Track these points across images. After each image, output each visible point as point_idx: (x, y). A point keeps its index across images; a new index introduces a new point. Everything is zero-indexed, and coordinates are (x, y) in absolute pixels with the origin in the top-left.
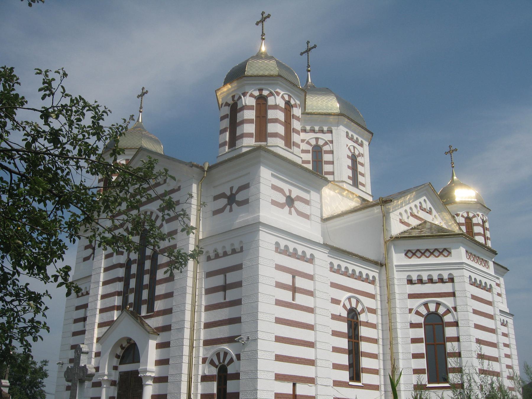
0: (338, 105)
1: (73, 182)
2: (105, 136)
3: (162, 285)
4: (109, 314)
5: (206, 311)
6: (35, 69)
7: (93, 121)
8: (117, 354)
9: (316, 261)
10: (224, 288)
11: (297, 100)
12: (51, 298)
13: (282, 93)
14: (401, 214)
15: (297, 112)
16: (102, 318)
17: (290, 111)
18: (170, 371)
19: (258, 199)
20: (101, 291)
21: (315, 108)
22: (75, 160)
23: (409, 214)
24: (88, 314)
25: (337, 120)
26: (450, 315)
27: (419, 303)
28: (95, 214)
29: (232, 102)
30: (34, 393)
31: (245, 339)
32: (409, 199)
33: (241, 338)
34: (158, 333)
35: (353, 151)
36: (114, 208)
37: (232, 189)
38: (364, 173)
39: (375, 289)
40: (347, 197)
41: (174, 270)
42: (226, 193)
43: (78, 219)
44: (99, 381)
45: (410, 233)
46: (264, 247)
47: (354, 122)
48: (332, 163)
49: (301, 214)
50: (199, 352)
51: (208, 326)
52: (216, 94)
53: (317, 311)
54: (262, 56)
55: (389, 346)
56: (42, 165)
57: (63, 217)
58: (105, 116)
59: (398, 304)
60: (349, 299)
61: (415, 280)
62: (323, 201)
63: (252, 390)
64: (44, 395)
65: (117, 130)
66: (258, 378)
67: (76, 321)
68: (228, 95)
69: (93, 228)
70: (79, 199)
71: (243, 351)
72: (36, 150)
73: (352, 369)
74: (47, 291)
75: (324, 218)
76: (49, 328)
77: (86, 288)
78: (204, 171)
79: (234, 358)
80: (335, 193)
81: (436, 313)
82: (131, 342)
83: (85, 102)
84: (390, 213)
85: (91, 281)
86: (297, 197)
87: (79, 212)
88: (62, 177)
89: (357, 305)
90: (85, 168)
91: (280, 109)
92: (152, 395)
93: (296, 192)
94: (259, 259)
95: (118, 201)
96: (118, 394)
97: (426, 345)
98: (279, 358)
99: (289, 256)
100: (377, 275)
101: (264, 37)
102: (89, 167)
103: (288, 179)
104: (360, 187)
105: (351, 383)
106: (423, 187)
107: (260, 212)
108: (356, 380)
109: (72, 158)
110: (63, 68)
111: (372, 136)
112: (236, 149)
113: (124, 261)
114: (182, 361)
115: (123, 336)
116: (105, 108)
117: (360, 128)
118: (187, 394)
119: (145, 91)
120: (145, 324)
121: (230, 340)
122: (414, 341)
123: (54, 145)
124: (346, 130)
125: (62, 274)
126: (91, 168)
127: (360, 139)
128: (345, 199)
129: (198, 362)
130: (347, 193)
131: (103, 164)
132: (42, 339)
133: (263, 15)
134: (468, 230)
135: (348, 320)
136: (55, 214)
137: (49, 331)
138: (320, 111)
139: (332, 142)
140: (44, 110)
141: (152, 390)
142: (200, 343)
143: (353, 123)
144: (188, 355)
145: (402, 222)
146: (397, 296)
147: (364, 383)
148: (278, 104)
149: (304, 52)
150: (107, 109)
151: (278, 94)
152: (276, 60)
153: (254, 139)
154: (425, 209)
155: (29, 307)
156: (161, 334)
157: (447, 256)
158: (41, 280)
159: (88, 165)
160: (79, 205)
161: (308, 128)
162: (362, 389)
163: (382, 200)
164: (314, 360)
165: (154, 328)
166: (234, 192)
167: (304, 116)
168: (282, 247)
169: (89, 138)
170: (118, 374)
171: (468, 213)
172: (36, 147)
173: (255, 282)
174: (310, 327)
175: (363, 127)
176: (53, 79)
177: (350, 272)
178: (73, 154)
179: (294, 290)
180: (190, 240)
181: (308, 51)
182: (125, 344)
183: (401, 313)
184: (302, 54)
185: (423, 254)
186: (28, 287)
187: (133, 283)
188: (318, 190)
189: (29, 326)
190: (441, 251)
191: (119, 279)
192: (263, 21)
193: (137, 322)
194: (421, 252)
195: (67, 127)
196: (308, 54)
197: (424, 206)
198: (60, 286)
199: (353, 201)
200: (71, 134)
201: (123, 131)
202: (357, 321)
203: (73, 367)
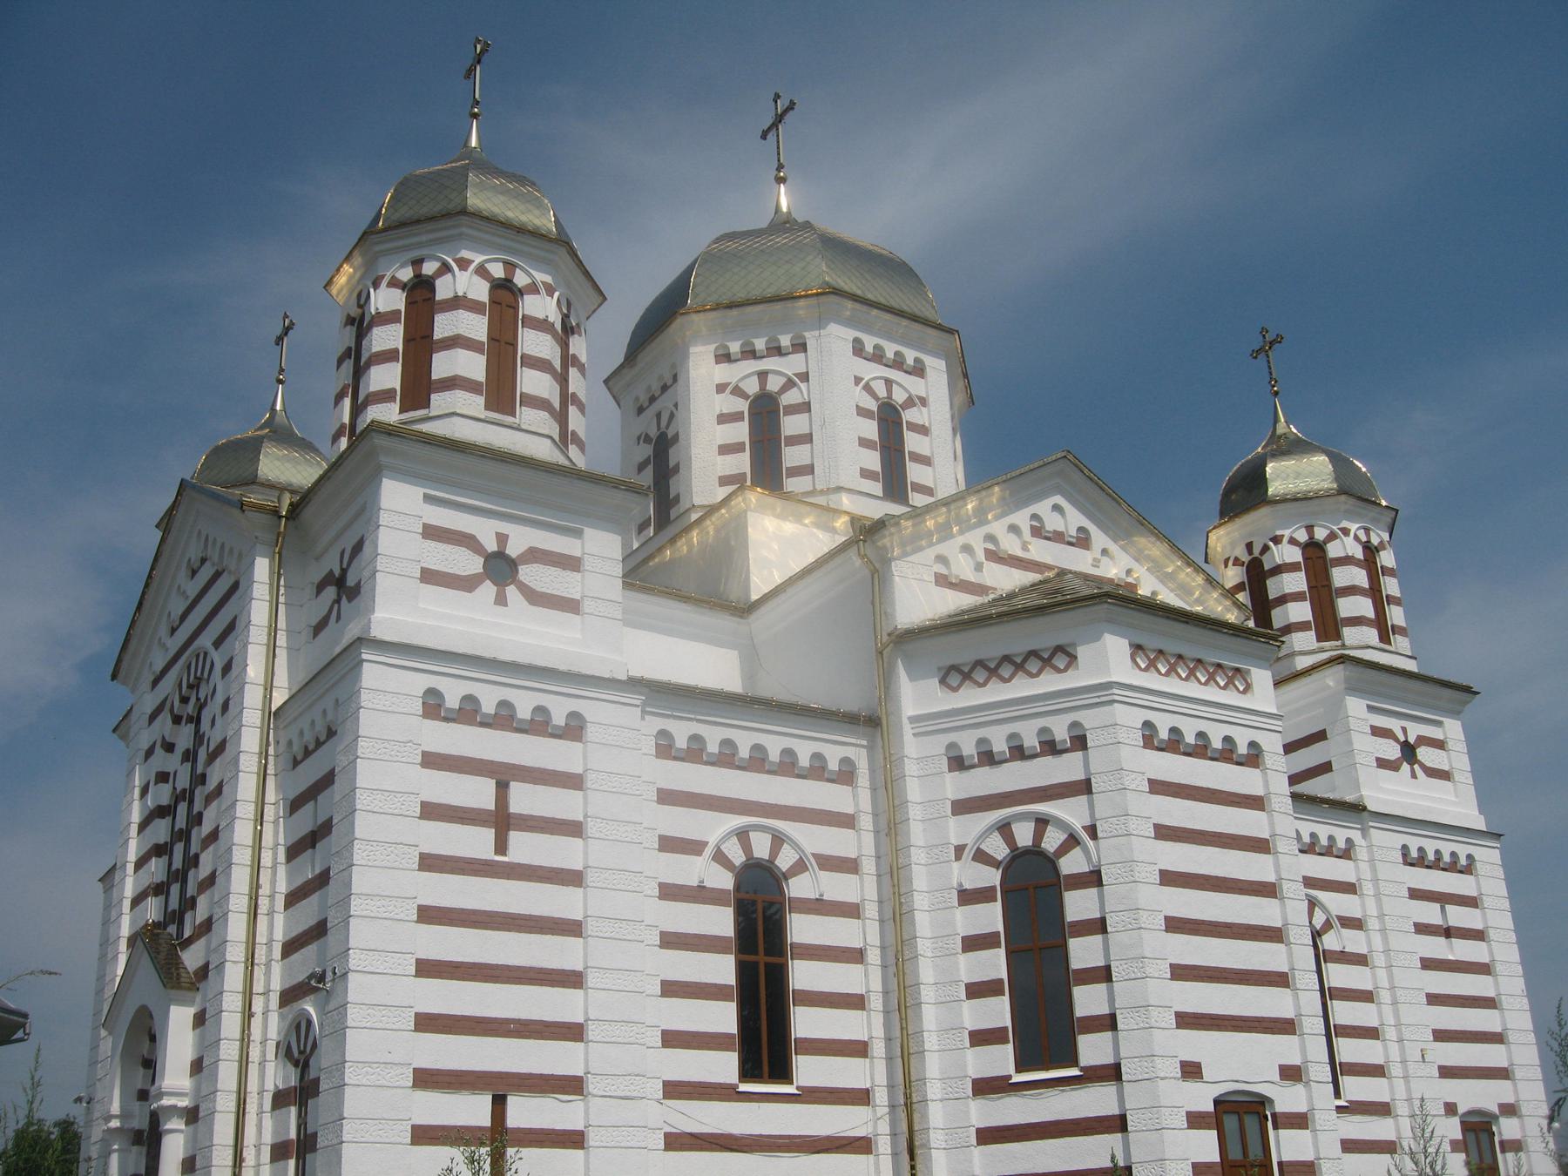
9: (591, 732)
11: (533, 269)
17: (514, 308)
23: (981, 556)
26: (1076, 852)
27: (983, 825)
39: (855, 796)
49: (535, 598)
60: (743, 835)
78: (280, 517)
80: (800, 527)
81: (1035, 851)
91: (475, 307)
97: (1009, 954)
105: (744, 1087)
117: (905, 322)
124: (851, 334)
127: (910, 356)
134: (1314, 584)
139: (805, 377)
145: (942, 581)
147: (801, 1084)
148: (460, 294)
149: (770, 129)
153: (396, 407)
157: (1065, 670)
161: (735, 347)
171: (1310, 529)
190: (966, 670)
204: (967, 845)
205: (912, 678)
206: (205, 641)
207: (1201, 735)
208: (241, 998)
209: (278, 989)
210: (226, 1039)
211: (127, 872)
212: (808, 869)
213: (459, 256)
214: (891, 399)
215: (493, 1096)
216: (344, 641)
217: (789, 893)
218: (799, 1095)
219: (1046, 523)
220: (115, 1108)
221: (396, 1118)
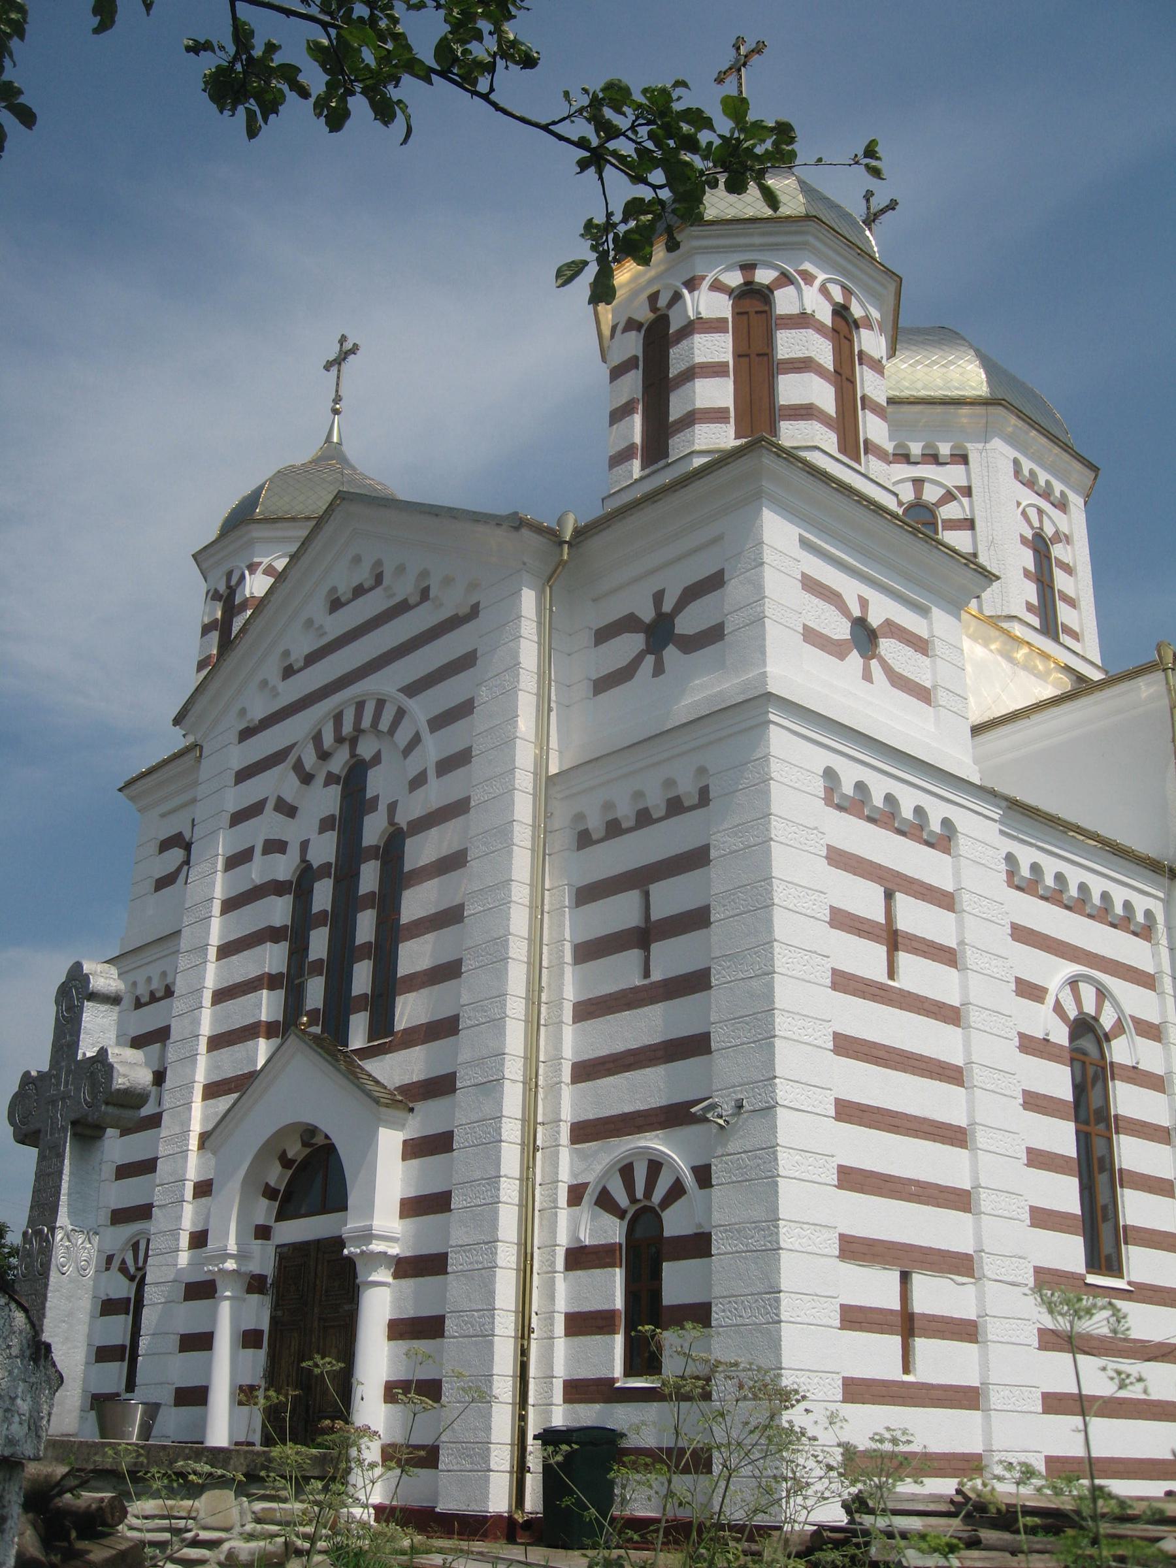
4: (238, 1050)
5: (579, 1021)
9: (963, 844)
13: (821, 277)
16: (218, 1067)
17: (849, 340)
19: (759, 620)
20: (212, 976)
21: (907, 384)
25: (985, 421)
29: (651, 316)
31: (727, 1108)
33: (713, 1107)
34: (411, 1105)
35: (1036, 524)
37: (658, 597)
38: (1074, 596)
39: (1155, 955)
40: (1027, 668)
42: (637, 613)
44: (209, 1277)
50: (555, 1165)
51: (586, 1071)
60: (1073, 983)
63: (759, 1293)
66: (780, 1248)
71: (719, 1152)
77: (164, 974)
79: (689, 1179)
82: (314, 1141)
89: (1099, 1007)
92: (390, 1320)
93: (881, 610)
94: (769, 823)
96: (274, 1320)
103: (855, 560)
105: (1092, 1279)
107: (769, 661)
112: (669, 465)
117: (1057, 450)
119: (350, 346)
127: (1058, 487)
128: (1022, 673)
129: (555, 1201)
130: (1026, 655)
139: (968, 491)
141: (392, 1302)
142: (558, 1133)
143: (1034, 433)
144: (518, 1176)
148: (809, 311)
151: (809, 278)
153: (730, 429)
156: (419, 1106)
162: (1130, 1300)
165: (396, 1089)
166: (667, 607)
168: (848, 789)
173: (762, 907)
177: (1073, 891)
182: (295, 1150)
187: (319, 944)
191: (272, 934)
199: (1045, 681)
206: (386, 682)
209: (569, 1119)
210: (505, 1176)
213: (801, 268)
214: (1042, 530)
215: (902, 1272)
216: (687, 701)
218: (1131, 1291)
220: (232, 1248)
221: (826, 1294)
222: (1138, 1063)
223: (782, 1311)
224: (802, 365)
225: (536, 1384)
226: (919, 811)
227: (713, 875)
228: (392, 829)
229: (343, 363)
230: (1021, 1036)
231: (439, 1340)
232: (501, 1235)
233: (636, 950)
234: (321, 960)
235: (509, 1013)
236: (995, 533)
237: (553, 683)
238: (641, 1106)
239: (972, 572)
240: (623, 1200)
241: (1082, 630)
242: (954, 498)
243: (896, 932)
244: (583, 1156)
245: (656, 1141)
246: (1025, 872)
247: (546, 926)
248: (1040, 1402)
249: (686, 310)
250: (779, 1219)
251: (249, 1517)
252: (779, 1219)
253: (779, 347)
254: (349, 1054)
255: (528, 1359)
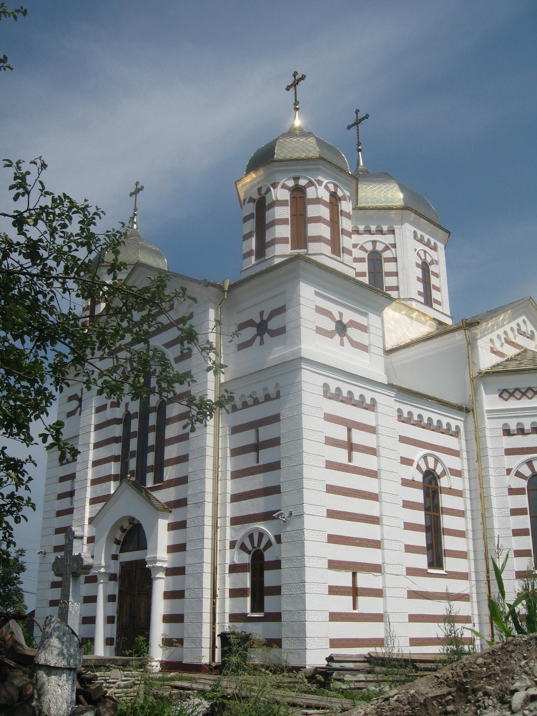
0: (401, 196)
1: (59, 310)
2: (100, 247)
3: (173, 446)
4: (103, 486)
6: (4, 160)
7: (81, 227)
8: (116, 539)
9: (379, 408)
10: (257, 447)
12: (36, 465)
14: (492, 341)
15: (346, 206)
17: (337, 206)
18: (188, 559)
19: (298, 327)
22: (60, 280)
23: (503, 341)
24: (76, 487)
25: (401, 216)
28: (88, 351)
30: (9, 592)
31: (286, 515)
32: (503, 320)
33: (281, 514)
34: (170, 510)
35: (423, 258)
36: (111, 344)
37: (262, 313)
39: (460, 443)
40: (417, 320)
41: (195, 423)
43: (65, 360)
44: (94, 574)
45: (505, 366)
46: (308, 390)
47: (423, 218)
48: (396, 274)
49: (355, 344)
50: (225, 533)
51: (236, 498)
52: (236, 186)
53: (383, 474)
54: (296, 133)
55: (480, 520)
56: (16, 289)
57: (46, 358)
58: (97, 220)
59: (491, 463)
60: (425, 457)
61: (514, 430)
62: (385, 327)
64: (22, 594)
65: (113, 237)
66: (305, 567)
67: (61, 496)
68: (252, 187)
69: (86, 371)
70: (68, 334)
71: (284, 531)
72: (8, 269)
73: (430, 551)
74: (30, 457)
75: (387, 349)
76: (35, 505)
79: (273, 540)
80: (400, 315)
83: (71, 202)
84: (477, 339)
85: (78, 443)
86: (351, 321)
87: (66, 350)
88: (44, 303)
90: (74, 291)
91: (324, 203)
92: (164, 592)
93: (348, 316)
95: (120, 333)
96: (120, 591)
98: (333, 539)
99: (342, 401)
100: (461, 425)
101: (297, 106)
102: (80, 289)
104: (435, 306)
105: (430, 571)
106: (521, 303)
108: (437, 567)
109: (56, 278)
110: (41, 157)
111: (449, 236)
113: (122, 415)
114: (203, 546)
115: (120, 517)
116: (97, 209)
117: (432, 226)
118: (211, 589)
119: (140, 187)
120: (152, 498)
121: (267, 516)
122: (515, 512)
123: (32, 261)
124: (413, 229)
125: (53, 432)
126: (83, 290)
127: (433, 241)
128: (416, 322)
129: (225, 547)
131: (98, 284)
132: (27, 520)
133: (295, 77)
135: (424, 487)
136: (36, 354)
137: (34, 509)
138: (377, 204)
139: (394, 246)
140: (18, 215)
142: (226, 521)
143: (422, 220)
145: (494, 351)
146: (490, 453)
148: (320, 197)
149: (353, 125)
150: (100, 210)
151: (320, 183)
152: (315, 137)
153: (289, 246)
154: (524, 332)
155: (8, 479)
156: (173, 510)
158: (22, 442)
159: (79, 286)
160: (68, 340)
161: (362, 228)
163: (466, 322)
164: (380, 541)
165: (165, 503)
167: (355, 211)
168: (333, 390)
169: (76, 250)
170: (118, 565)
172: (8, 265)
173: (298, 439)
174: (373, 497)
175: (436, 225)
176: (28, 173)
178: (58, 273)
179: (350, 447)
180: (208, 384)
181: (357, 123)
182: (126, 526)
183: (496, 475)
184: (349, 127)
185: (524, 394)
186: (5, 451)
187: (134, 444)
188: (379, 311)
189: (8, 504)
190: (511, 391)
191: (115, 440)
192: (295, 84)
193: (141, 495)
194: (509, 393)
195: (48, 236)
196: (358, 127)
197: (523, 329)
198: (51, 448)
199: (425, 325)
200: (54, 245)
201: (122, 238)
202: (436, 487)
203: (64, 556)
204: (512, 469)
205: (486, 394)
207: (350, 393)
208: (211, 519)
210: (206, 538)
211: (90, 448)
212: (446, 475)
215: (353, 573)
217: (440, 484)
219: (521, 327)
220: (103, 564)
222: (451, 486)
223: (306, 589)
224: (317, 220)
225: (219, 615)
226: (362, 396)
227: (281, 426)
228: (161, 400)
229: (137, 194)
230: (402, 479)
231: (183, 599)
232: (205, 560)
233: (254, 453)
234: (135, 451)
235: (206, 476)
236: (405, 263)
237: (222, 346)
238: (256, 512)
239: (385, 298)
240: (250, 547)
241: (442, 301)
242: (389, 249)
243: (352, 444)
244: (235, 530)
245: (261, 525)
246: (405, 415)
247: (220, 442)
248: (408, 618)
249: (272, 197)
250: (305, 556)
251: (123, 676)
252: (305, 556)
253: (308, 212)
254: (147, 489)
255: (216, 606)
